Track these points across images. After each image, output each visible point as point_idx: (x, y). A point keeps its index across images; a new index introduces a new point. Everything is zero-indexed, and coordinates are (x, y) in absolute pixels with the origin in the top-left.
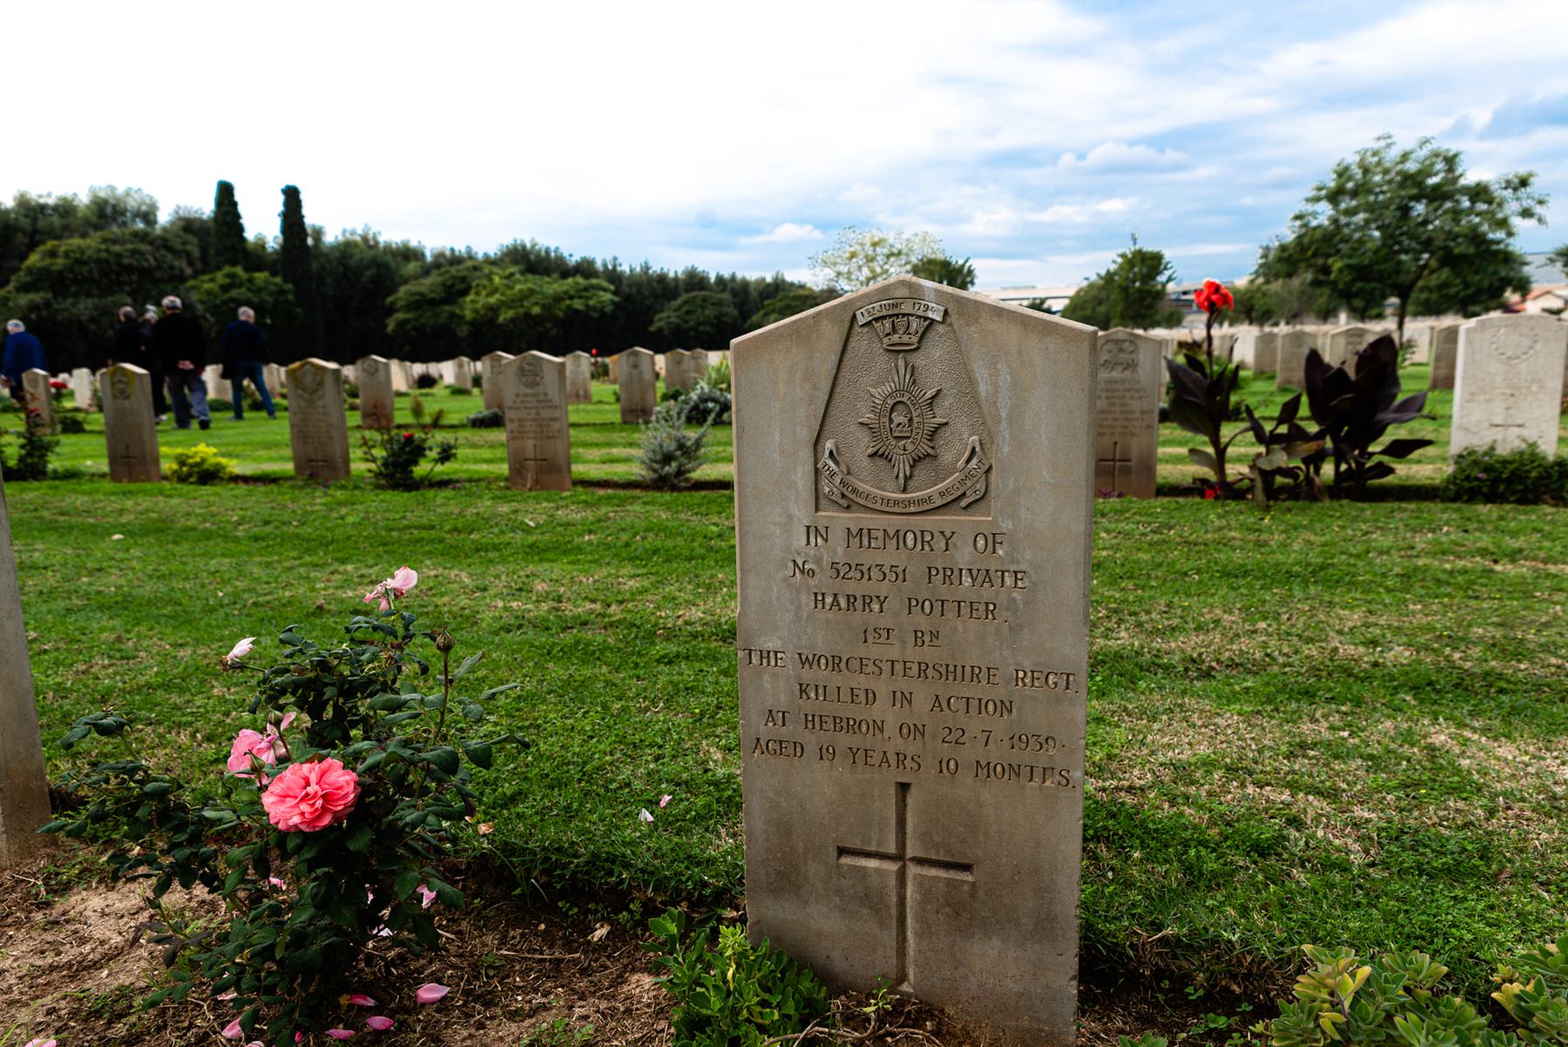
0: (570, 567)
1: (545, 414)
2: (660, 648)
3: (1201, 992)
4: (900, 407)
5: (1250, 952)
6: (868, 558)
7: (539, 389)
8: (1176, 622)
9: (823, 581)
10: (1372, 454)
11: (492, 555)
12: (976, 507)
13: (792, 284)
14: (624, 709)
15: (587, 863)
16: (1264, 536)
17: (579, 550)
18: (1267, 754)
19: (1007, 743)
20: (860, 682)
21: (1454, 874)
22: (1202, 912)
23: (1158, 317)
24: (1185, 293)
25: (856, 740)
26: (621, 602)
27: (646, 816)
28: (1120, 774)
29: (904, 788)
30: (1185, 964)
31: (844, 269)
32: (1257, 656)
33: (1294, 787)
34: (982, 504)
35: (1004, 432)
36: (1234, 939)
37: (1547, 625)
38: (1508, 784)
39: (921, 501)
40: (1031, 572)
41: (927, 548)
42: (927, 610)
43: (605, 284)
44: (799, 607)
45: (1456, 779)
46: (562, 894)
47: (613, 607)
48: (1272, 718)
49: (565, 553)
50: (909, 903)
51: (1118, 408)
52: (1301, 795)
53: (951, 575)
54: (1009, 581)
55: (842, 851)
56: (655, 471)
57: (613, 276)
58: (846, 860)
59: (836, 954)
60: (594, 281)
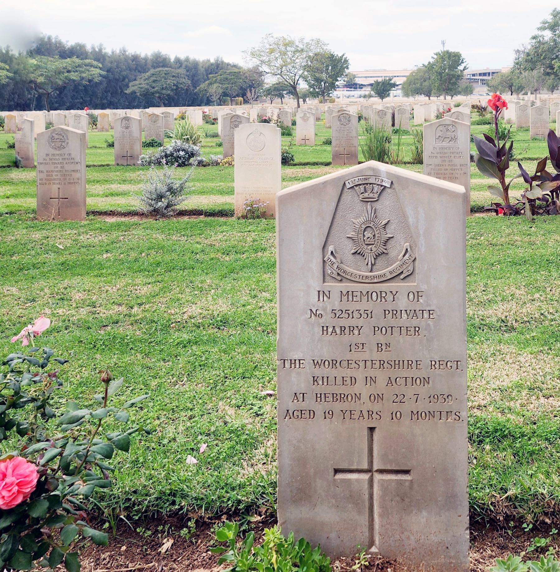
0: (96, 280)
1: (68, 167)
2: (176, 336)
3: (531, 526)
4: (369, 229)
5: (553, 499)
6: (352, 307)
7: (66, 151)
8: (491, 296)
9: (328, 320)
11: (32, 272)
12: (408, 279)
13: (228, 64)
14: (159, 386)
15: (157, 499)
16: (533, 238)
17: (101, 266)
18: (548, 377)
22: (527, 478)
23: (460, 89)
24: (474, 75)
25: (345, 406)
26: (140, 305)
27: (191, 460)
28: (472, 398)
30: (520, 510)
31: (265, 59)
32: (536, 316)
34: (411, 277)
35: (422, 241)
36: (545, 492)
39: (380, 276)
40: (437, 310)
41: (383, 300)
43: (95, 63)
46: (137, 524)
47: (136, 309)
48: (548, 354)
49: (90, 268)
50: (375, 497)
51: (447, 163)
53: (395, 313)
54: (426, 315)
55: (336, 471)
56: (151, 205)
57: (99, 56)
58: (340, 476)
59: (333, 535)
60: (87, 61)
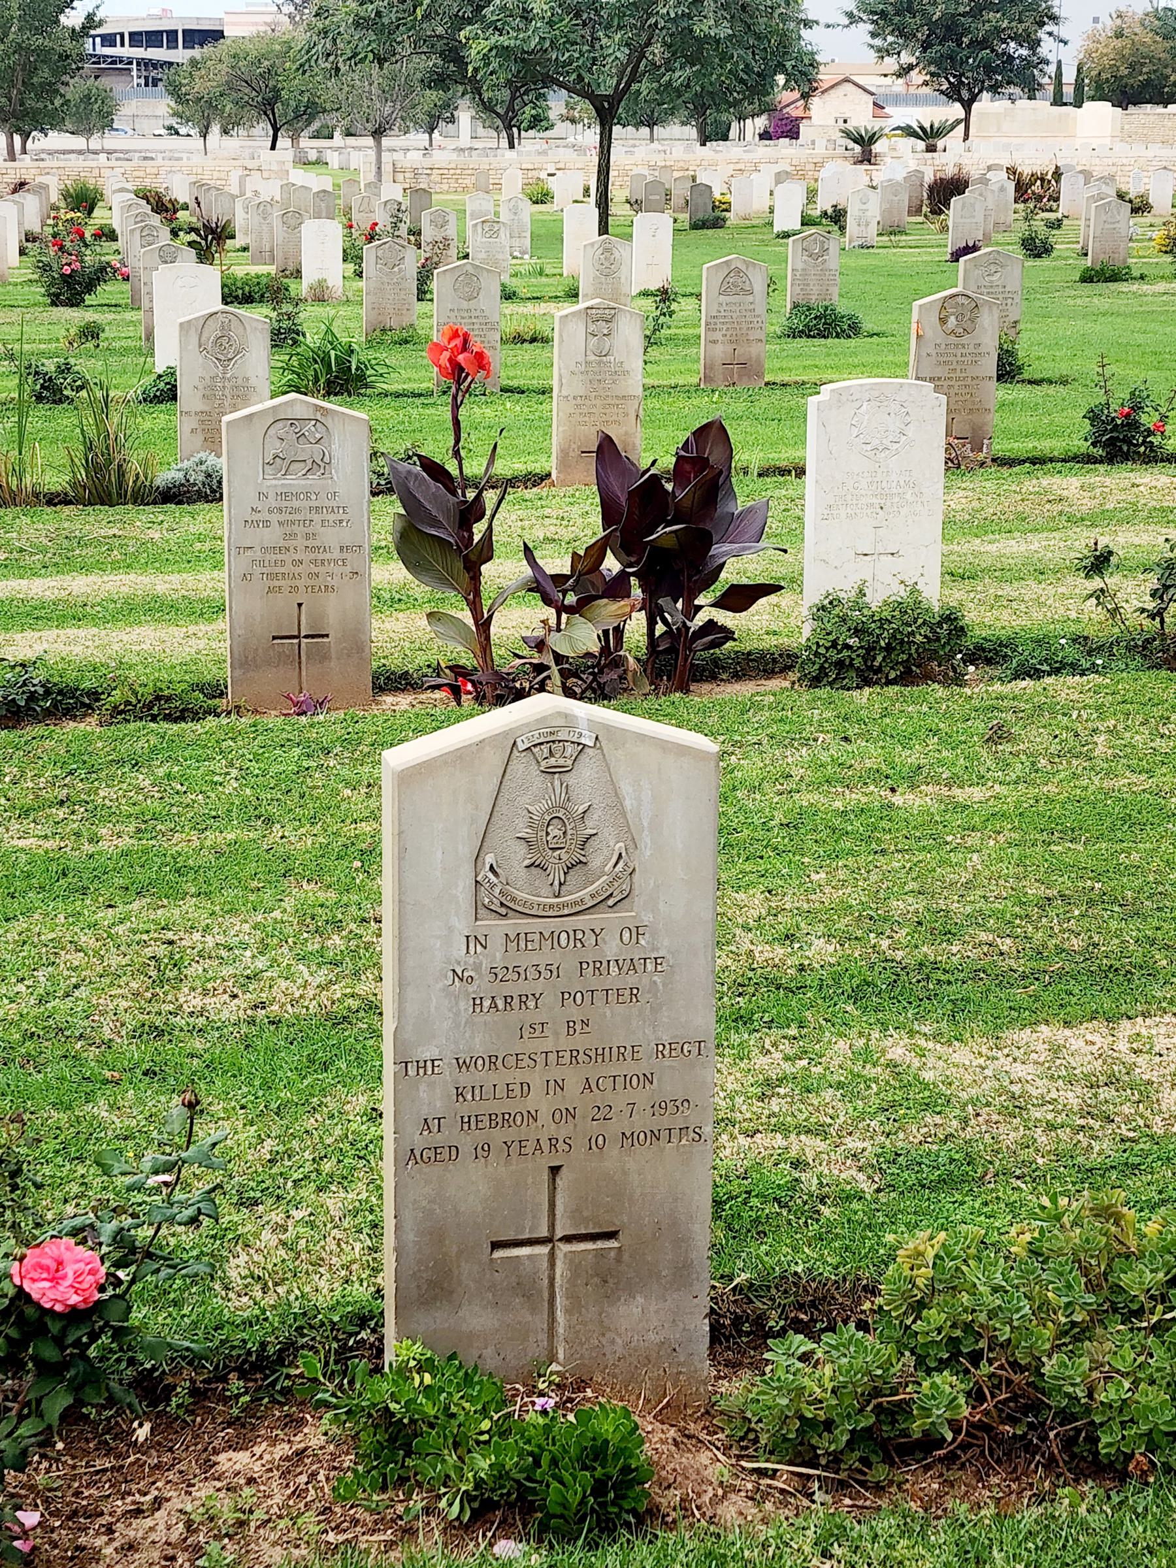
6: (525, 960)
9: (483, 986)
10: (700, 607)
18: (739, 1100)
19: (649, 1111)
20: (518, 1076)
21: (946, 1182)
25: (511, 1134)
29: (555, 1170)
33: (782, 1129)
35: (645, 840)
37: (968, 886)
38: (973, 1092)
40: (668, 956)
42: (579, 1001)
44: (458, 1014)
45: (927, 1093)
51: (300, 542)
52: (793, 1136)
53: (599, 967)
54: (650, 966)
55: (496, 1245)
58: (500, 1254)
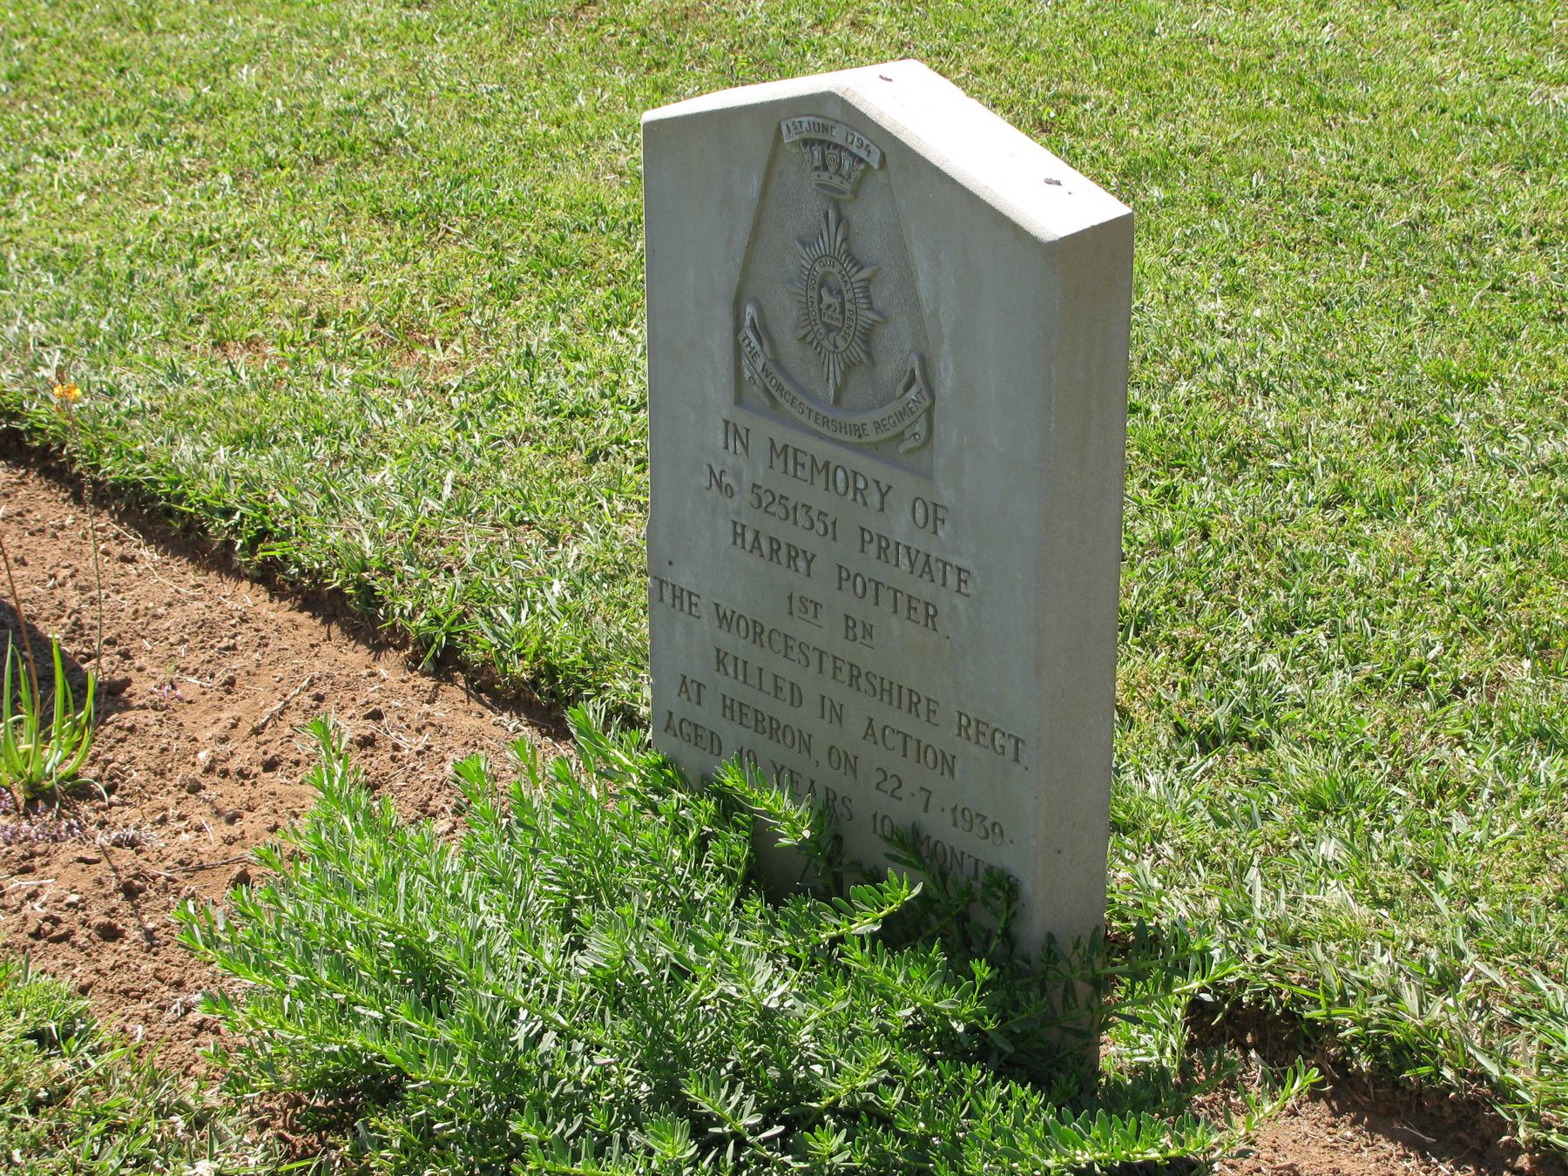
53: (886, 549)
54: (952, 579)
